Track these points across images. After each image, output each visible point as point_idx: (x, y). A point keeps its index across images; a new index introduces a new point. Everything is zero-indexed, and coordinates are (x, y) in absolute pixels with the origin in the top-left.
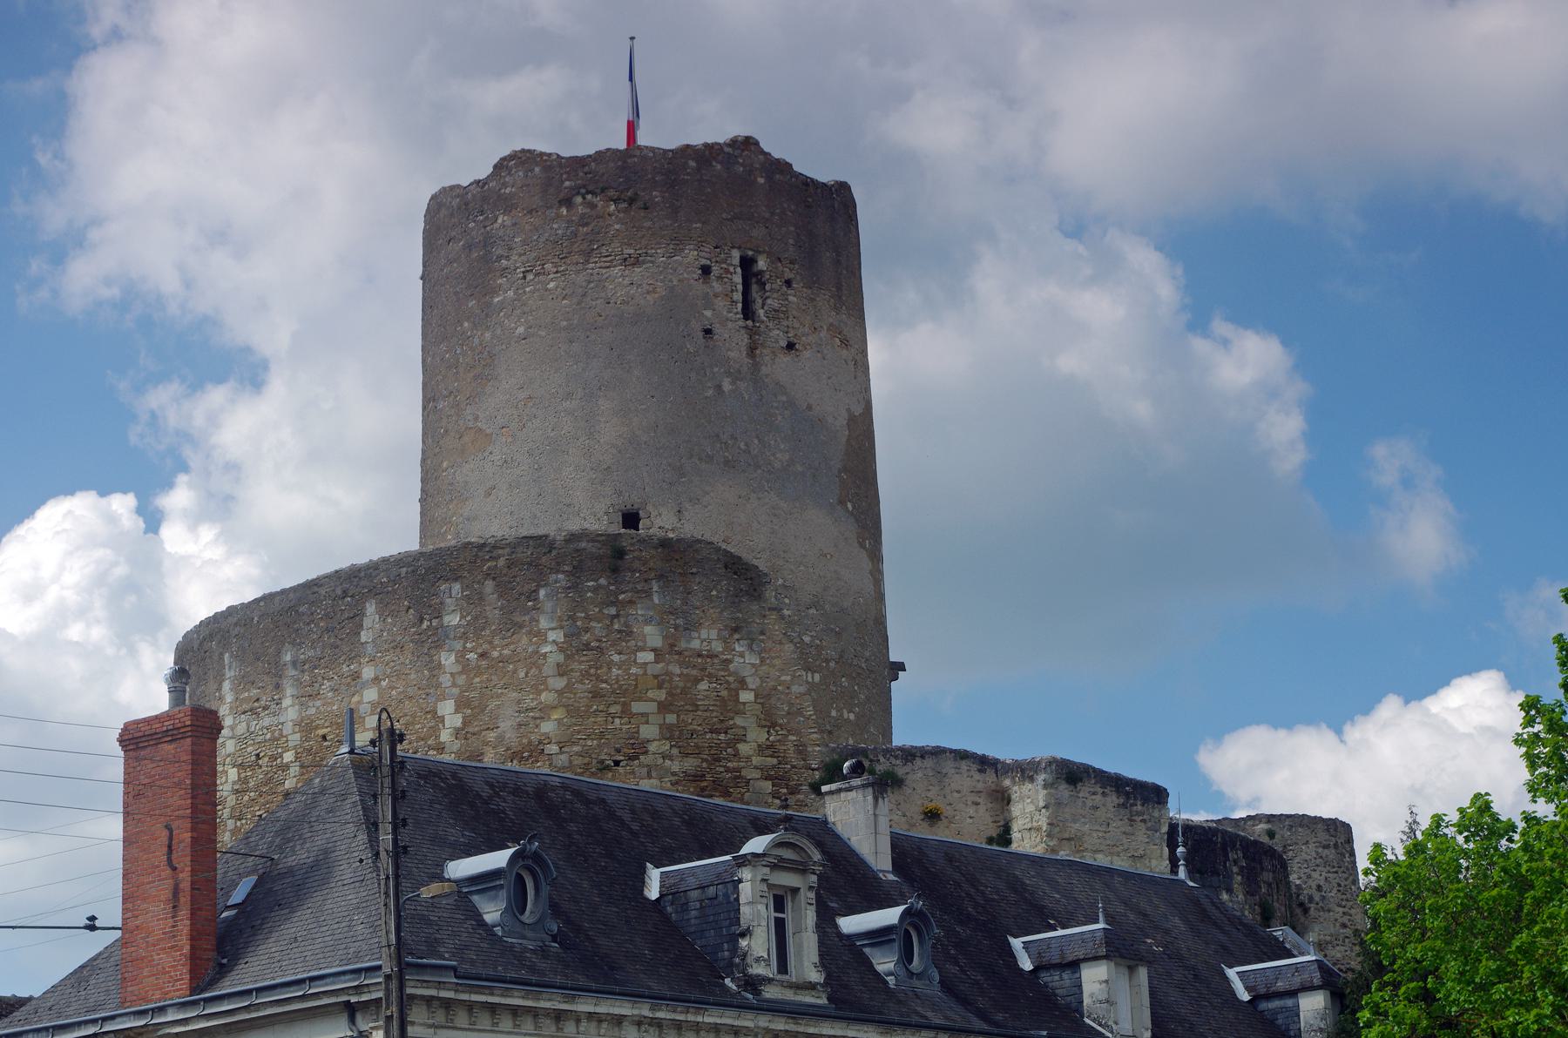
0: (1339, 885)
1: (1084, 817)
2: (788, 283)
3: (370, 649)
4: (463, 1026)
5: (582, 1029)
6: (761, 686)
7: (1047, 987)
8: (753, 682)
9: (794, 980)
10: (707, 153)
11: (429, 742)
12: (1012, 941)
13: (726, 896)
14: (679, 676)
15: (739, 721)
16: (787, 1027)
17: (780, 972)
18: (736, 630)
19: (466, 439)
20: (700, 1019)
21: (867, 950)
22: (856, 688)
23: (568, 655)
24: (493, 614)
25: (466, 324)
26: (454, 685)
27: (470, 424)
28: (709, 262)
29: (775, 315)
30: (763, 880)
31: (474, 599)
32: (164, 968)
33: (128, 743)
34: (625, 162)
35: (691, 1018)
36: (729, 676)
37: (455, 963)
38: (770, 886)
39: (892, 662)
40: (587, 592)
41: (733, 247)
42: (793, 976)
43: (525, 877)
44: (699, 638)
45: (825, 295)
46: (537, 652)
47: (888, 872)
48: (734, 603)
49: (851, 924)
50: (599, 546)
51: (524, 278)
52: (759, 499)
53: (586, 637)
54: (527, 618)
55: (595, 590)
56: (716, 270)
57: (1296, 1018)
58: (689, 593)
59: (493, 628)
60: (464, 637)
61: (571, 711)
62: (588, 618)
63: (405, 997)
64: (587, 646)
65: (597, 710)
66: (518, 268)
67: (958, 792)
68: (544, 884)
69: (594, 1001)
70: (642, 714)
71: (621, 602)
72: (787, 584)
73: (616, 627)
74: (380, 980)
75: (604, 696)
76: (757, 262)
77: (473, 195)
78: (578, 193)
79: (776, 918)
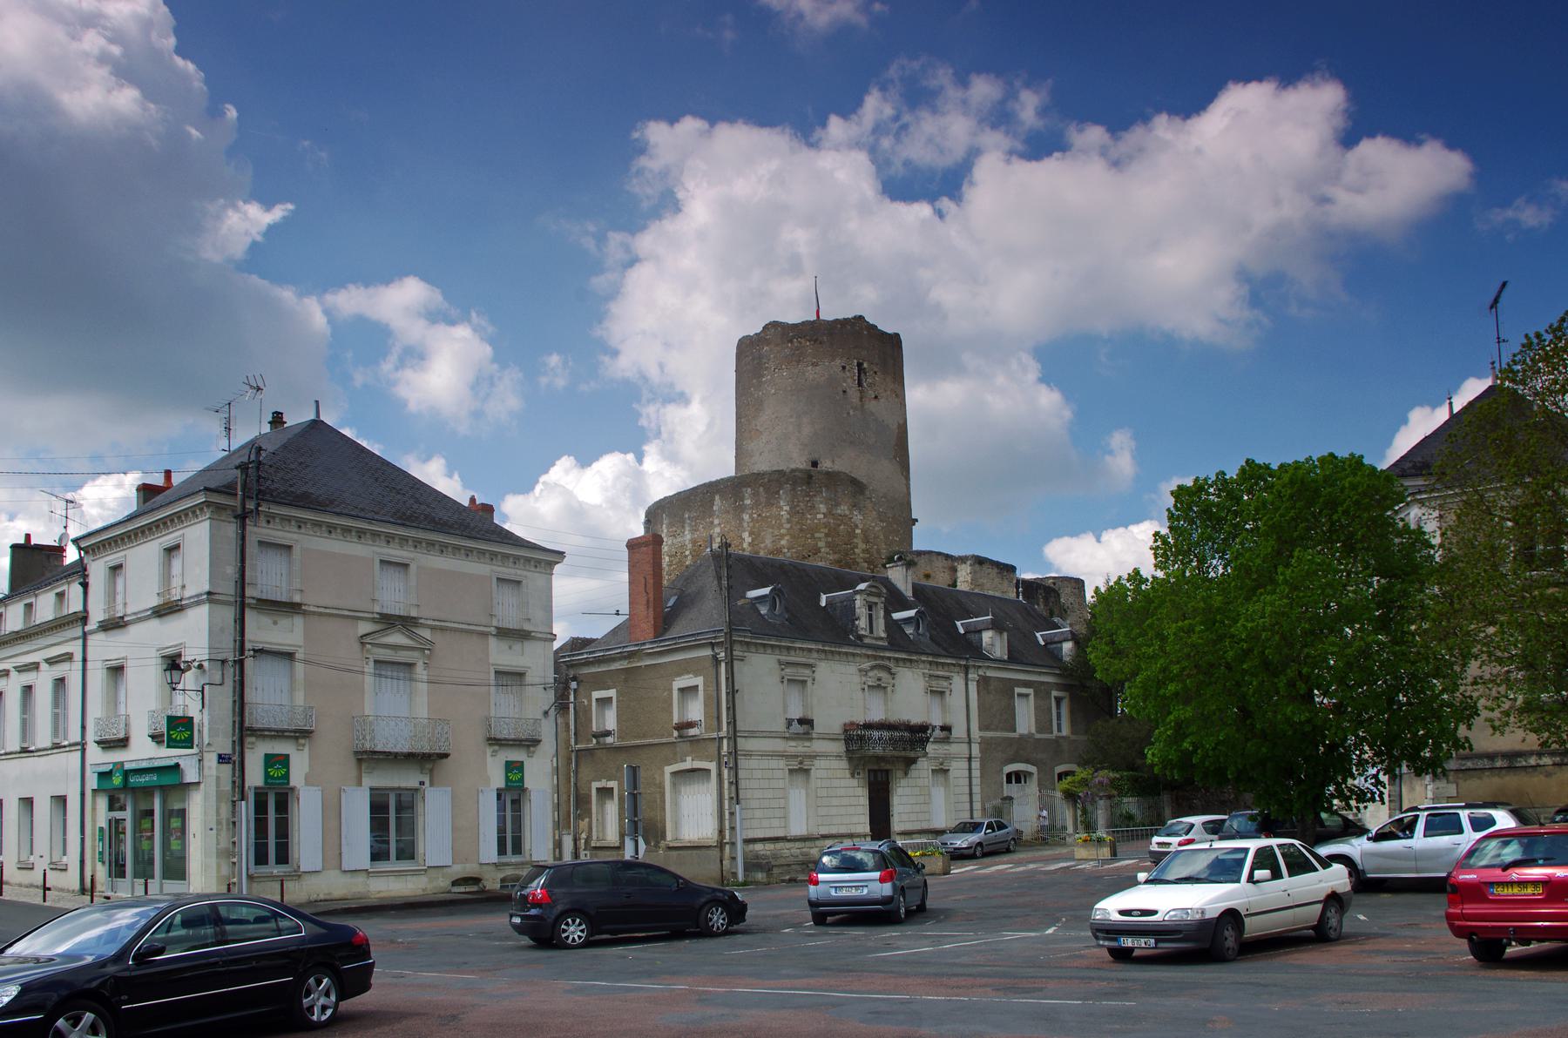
2: (875, 373)
8: (861, 526)
15: (855, 540)
24: (763, 500)
29: (870, 385)
31: (755, 495)
49: (897, 616)
53: (798, 509)
55: (801, 491)
61: (793, 537)
62: (799, 502)
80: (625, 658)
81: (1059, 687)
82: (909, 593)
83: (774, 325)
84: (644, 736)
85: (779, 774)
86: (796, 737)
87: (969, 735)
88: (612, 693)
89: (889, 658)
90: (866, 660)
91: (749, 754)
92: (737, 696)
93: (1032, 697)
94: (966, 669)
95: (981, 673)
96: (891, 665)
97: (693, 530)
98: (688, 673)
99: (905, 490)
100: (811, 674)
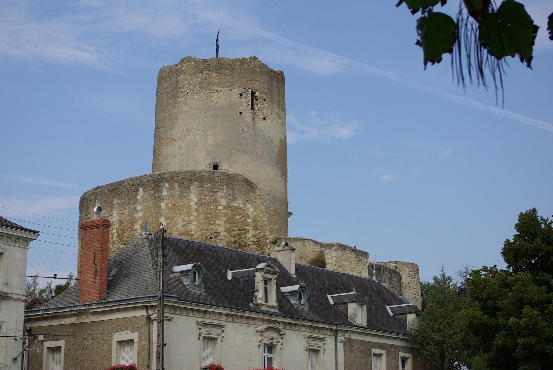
0: (414, 283)
1: (345, 260)
2: (265, 100)
3: (140, 201)
4: (179, 314)
5: (211, 316)
6: (254, 217)
7: (338, 309)
8: (252, 216)
9: (269, 305)
10: (243, 61)
11: (157, 229)
12: (328, 295)
13: (251, 280)
14: (230, 213)
15: (247, 228)
16: (267, 318)
17: (265, 302)
18: (247, 201)
19: (168, 140)
20: (243, 315)
21: (288, 297)
22: (278, 219)
23: (198, 206)
25: (169, 107)
26: (165, 213)
27: (169, 136)
28: (242, 93)
29: (260, 109)
30: (262, 276)
31: (171, 188)
32: (92, 293)
33: (83, 228)
35: (241, 314)
36: (245, 214)
37: (177, 296)
38: (264, 278)
39: (289, 212)
41: (249, 89)
42: (269, 303)
43: (196, 272)
44: (237, 203)
45: (275, 104)
46: (189, 204)
47: (294, 275)
48: (247, 193)
49: (284, 289)
50: (209, 175)
51: (188, 94)
53: (204, 201)
54: (187, 195)
57: (406, 321)
58: (234, 190)
59: (177, 197)
60: (168, 199)
61: (199, 222)
62: (205, 196)
63: (164, 305)
65: (206, 222)
66: (186, 91)
67: (309, 251)
68: (201, 274)
69: (225, 310)
71: (215, 191)
72: (260, 188)
73: (213, 198)
74: (157, 300)
76: (256, 93)
77: (173, 69)
78: (205, 70)
79: (265, 287)
80: (74, 315)
81: (405, 350)
82: (292, 271)
88: (61, 343)
89: (279, 322)
90: (262, 323)
92: (165, 348)
93: (384, 357)
94: (336, 332)
95: (347, 336)
96: (281, 327)
97: (121, 214)
98: (126, 330)
100: (221, 333)
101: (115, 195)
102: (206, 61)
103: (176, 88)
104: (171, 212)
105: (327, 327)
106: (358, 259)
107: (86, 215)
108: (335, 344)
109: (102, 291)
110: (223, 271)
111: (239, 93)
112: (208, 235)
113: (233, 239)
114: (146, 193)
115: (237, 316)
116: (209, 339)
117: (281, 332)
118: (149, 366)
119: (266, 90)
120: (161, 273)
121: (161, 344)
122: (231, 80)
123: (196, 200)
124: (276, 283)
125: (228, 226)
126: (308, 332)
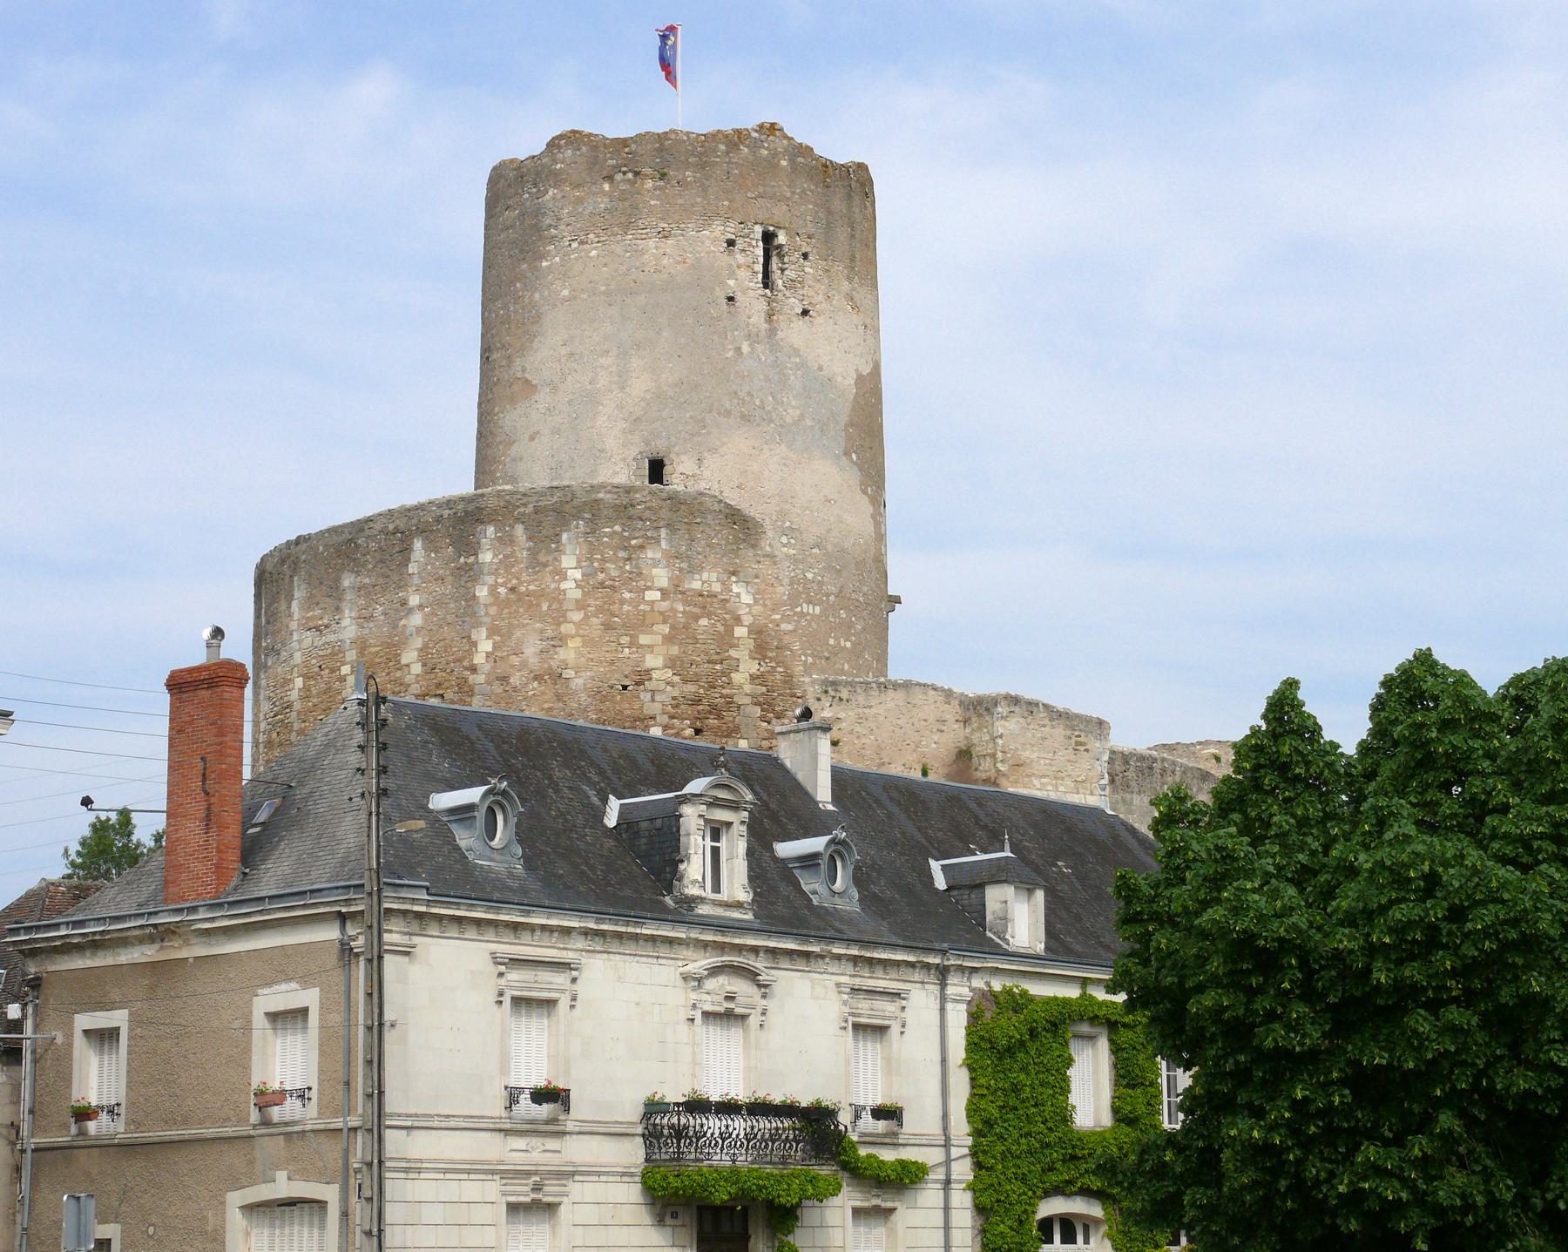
2: (805, 256)
3: (416, 580)
4: (434, 934)
8: (747, 620)
9: (726, 899)
10: (736, 138)
12: (932, 862)
15: (733, 653)
18: (733, 574)
20: (638, 931)
21: (796, 872)
25: (518, 285)
26: (487, 614)
28: (733, 237)
29: (792, 285)
31: (505, 540)
34: (662, 144)
35: (631, 930)
38: (707, 821)
40: (603, 537)
49: (785, 849)
52: (771, 450)
54: (550, 558)
56: (740, 244)
58: (693, 541)
60: (495, 573)
61: (588, 642)
62: (604, 560)
64: (602, 584)
67: (925, 720)
68: (511, 816)
70: (649, 646)
73: (628, 567)
75: (615, 629)
78: (620, 171)
80: (151, 939)
82: (823, 793)
83: (572, 138)
84: (186, 1122)
85: (482, 1214)
86: (531, 1130)
87: (945, 1128)
88: (118, 1018)
89: (755, 950)
91: (412, 1169)
92: (389, 1036)
94: (943, 973)
96: (759, 964)
97: (364, 618)
99: (870, 528)
101: (345, 562)
102: (624, 142)
103: (537, 228)
104: (506, 611)
105: (911, 958)
106: (1074, 739)
107: (268, 622)
108: (938, 1006)
109: (228, 868)
110: (595, 800)
111: (724, 238)
112: (616, 679)
113: (691, 688)
114: (433, 555)
115: (619, 936)
116: (534, 1003)
117: (760, 978)
118: (348, 1083)
119: (809, 225)
120: (374, 819)
121: (376, 1023)
122: (699, 200)
123: (578, 574)
124: (745, 834)
125: (675, 650)
126: (850, 976)
